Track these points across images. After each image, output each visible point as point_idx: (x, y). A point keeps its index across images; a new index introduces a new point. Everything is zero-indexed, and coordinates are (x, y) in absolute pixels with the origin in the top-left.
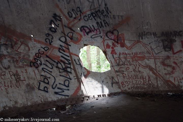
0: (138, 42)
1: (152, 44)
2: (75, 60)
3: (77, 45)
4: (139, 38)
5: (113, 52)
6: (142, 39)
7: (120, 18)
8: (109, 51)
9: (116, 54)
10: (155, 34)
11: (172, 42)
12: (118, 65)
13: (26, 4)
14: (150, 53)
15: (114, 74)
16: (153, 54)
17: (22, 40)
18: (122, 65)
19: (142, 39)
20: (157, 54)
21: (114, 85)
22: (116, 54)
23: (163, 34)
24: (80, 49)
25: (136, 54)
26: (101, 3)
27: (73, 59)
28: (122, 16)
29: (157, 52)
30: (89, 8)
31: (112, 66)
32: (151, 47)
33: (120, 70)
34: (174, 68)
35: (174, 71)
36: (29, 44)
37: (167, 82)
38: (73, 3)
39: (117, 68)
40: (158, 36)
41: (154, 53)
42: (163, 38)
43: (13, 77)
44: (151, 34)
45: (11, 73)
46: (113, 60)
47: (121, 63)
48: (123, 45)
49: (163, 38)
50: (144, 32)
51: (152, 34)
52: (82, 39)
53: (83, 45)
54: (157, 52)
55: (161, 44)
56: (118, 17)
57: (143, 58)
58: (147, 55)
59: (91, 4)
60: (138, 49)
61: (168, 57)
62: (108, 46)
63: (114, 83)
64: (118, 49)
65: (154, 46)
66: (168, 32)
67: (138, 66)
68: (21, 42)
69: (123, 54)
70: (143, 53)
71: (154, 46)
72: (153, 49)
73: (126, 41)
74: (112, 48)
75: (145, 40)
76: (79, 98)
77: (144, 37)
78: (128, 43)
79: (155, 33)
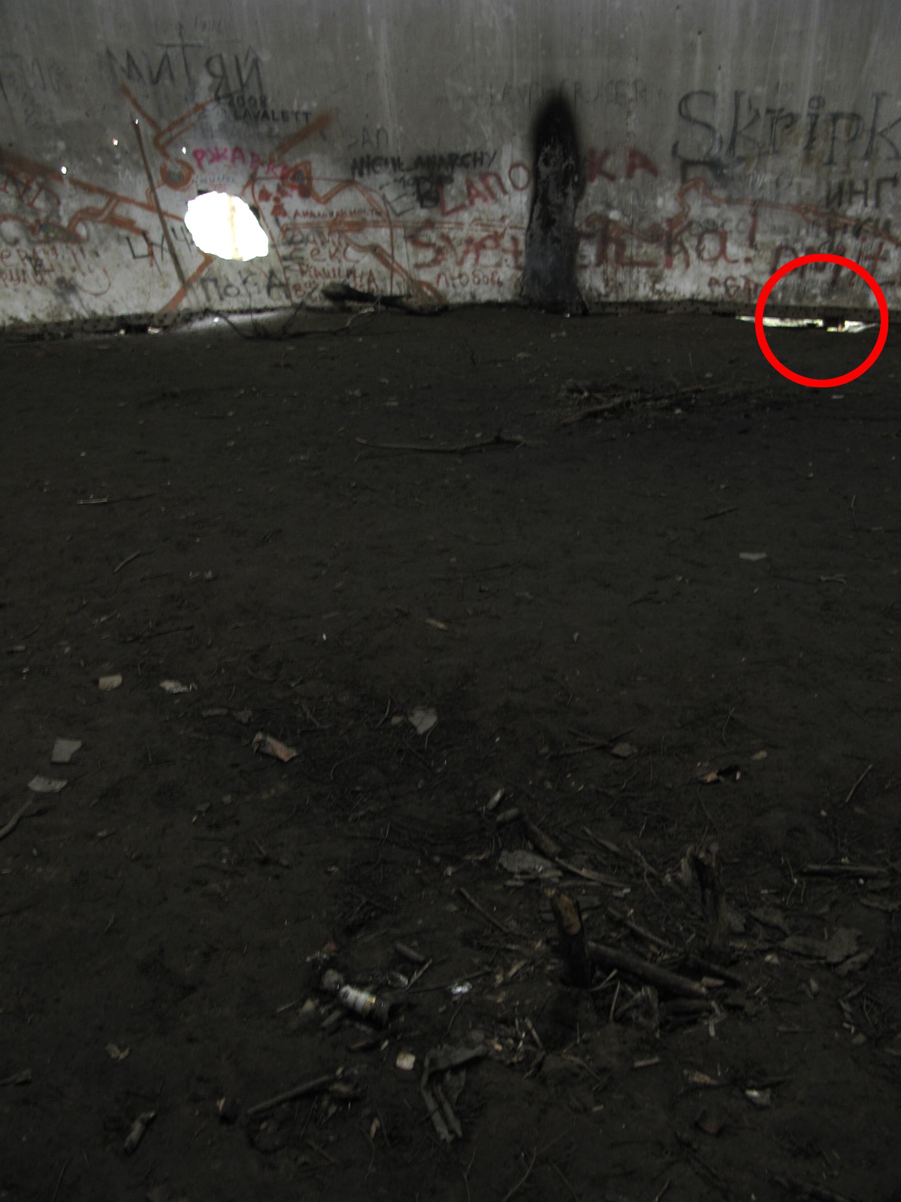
0: (349, 183)
1: (385, 188)
2: (173, 230)
3: (178, 193)
4: (353, 174)
5: (278, 211)
6: (361, 174)
7: (302, 118)
8: (267, 207)
9: (285, 214)
10: (397, 164)
11: (442, 181)
12: (290, 242)
13: (44, 88)
14: (379, 214)
15: (276, 264)
16: (388, 215)
17: (40, 180)
18: (301, 242)
19: (361, 174)
20: (398, 215)
21: (274, 291)
22: (285, 214)
23: (419, 162)
24: (186, 203)
25: (342, 214)
26: (249, 77)
27: (169, 228)
28: (306, 114)
29: (398, 210)
30: (213, 95)
31: (273, 246)
32: (384, 198)
33: (295, 255)
34: (439, 251)
35: (440, 257)
36: (596, 183)
37: (417, 285)
38: (167, 82)
39: (284, 251)
40: (405, 166)
41: (390, 212)
42: (418, 173)
43: (26, 261)
44: (386, 163)
45: (23, 255)
46: (276, 231)
47: (298, 238)
48: (306, 192)
49: (418, 173)
50: (368, 157)
51: (390, 160)
52: (194, 177)
53: (196, 192)
54: (398, 210)
55: (411, 189)
56: (297, 118)
57: (359, 226)
58: (369, 217)
59: (218, 80)
60: (348, 201)
61: (430, 224)
62: (265, 195)
63: (275, 285)
64: (294, 203)
65: (391, 195)
66: (434, 156)
67: (344, 245)
68: (38, 184)
69: (305, 214)
70: (362, 211)
71: (391, 195)
72: (389, 203)
73: (314, 182)
74: (277, 200)
75: (369, 180)
76: (325, 960)
77: (365, 171)
78: (321, 188)
79: (399, 159)
